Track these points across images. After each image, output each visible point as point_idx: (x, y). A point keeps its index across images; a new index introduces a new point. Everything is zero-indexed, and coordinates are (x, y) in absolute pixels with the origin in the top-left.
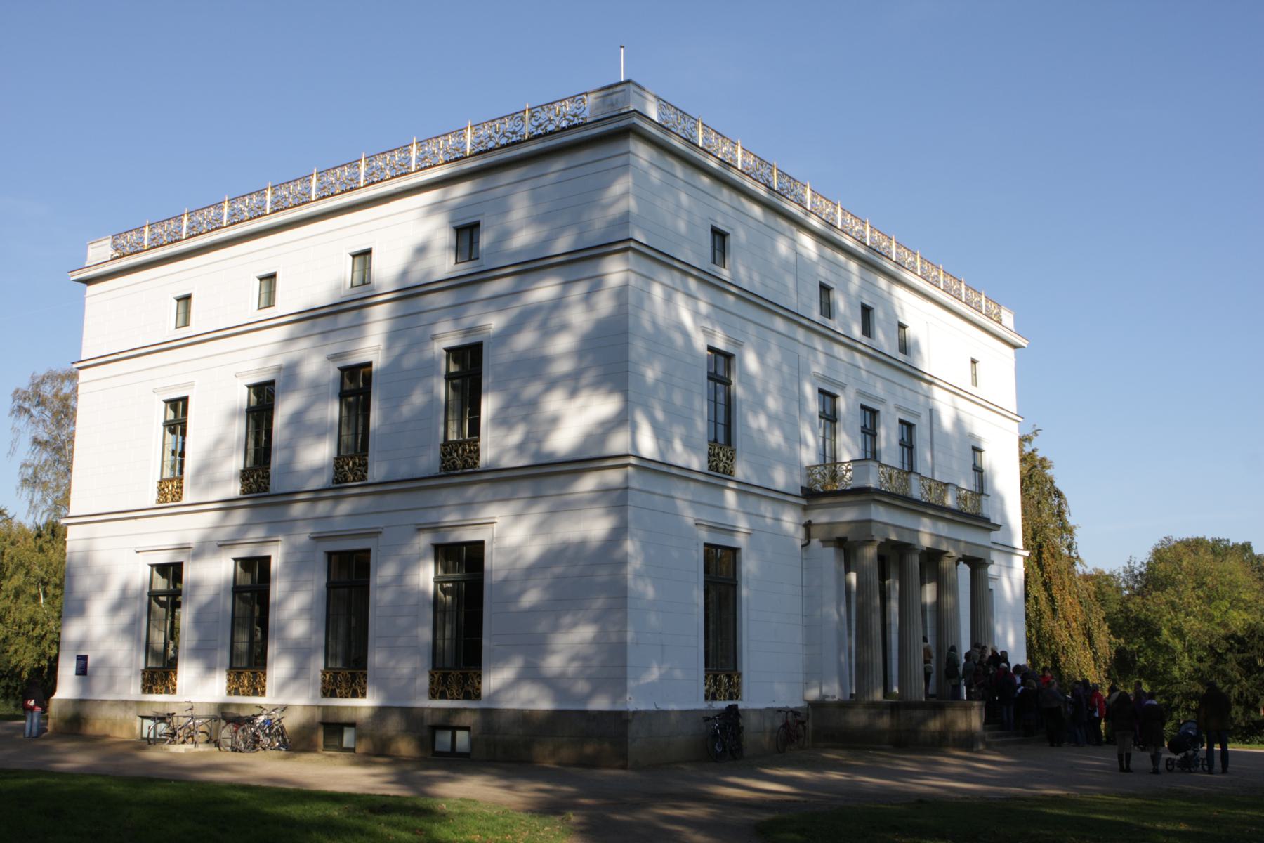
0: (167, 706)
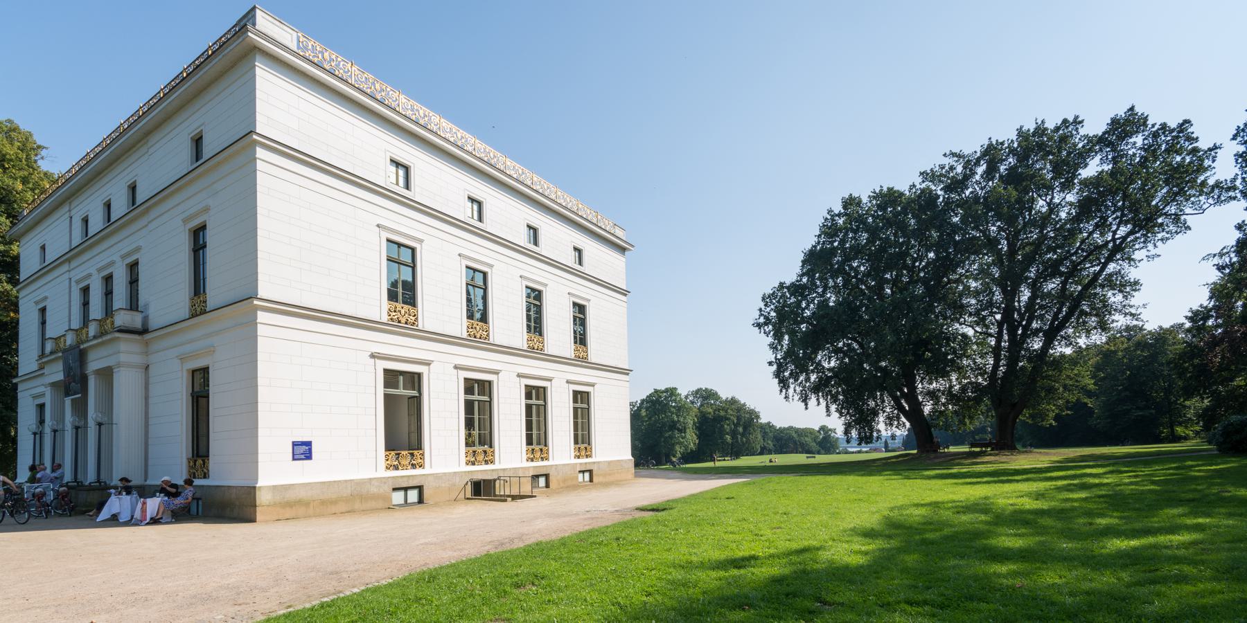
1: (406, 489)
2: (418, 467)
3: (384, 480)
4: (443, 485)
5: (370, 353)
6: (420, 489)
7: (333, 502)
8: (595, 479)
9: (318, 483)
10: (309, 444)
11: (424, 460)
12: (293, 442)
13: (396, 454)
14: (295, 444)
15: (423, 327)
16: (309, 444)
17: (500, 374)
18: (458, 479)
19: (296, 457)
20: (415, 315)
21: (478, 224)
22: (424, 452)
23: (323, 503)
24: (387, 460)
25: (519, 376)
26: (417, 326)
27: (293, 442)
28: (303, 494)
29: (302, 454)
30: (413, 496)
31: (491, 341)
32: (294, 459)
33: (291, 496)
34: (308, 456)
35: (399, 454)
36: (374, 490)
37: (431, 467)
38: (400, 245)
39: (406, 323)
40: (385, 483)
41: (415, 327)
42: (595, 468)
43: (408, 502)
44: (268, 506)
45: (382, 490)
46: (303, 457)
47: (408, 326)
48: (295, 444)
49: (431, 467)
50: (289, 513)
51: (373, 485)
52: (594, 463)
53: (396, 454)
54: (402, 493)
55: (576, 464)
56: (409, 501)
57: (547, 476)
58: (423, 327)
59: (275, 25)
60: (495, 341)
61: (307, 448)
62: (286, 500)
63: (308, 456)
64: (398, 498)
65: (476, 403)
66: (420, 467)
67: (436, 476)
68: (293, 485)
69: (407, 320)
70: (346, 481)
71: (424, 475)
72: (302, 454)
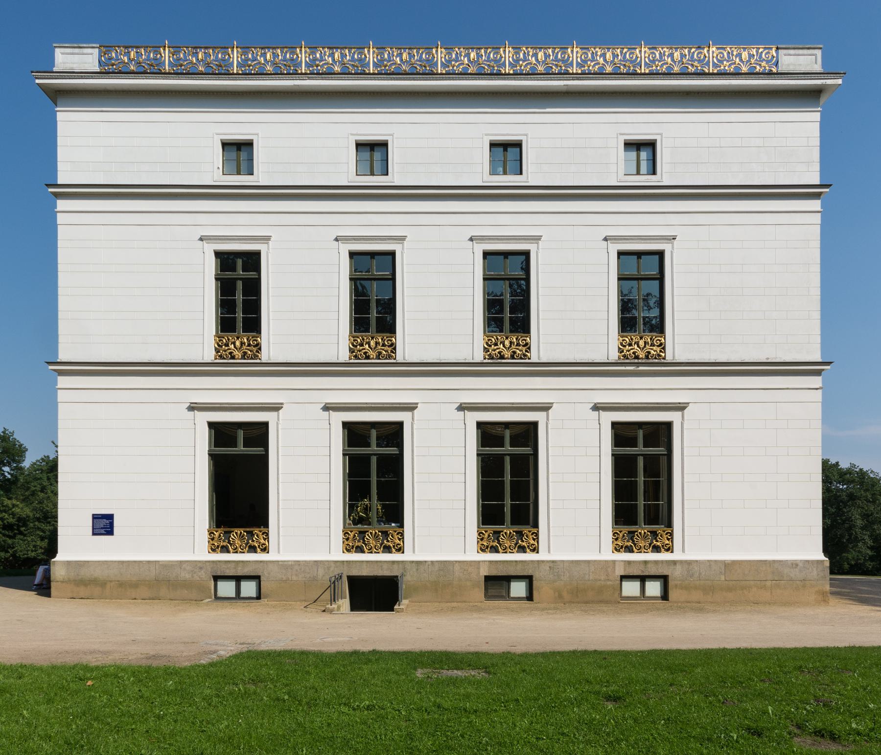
0: (649, 565)
1: (238, 579)
2: (394, 550)
3: (199, 565)
4: (294, 578)
5: (457, 405)
6: (529, 579)
7: (135, 585)
8: (672, 594)
9: (115, 561)
10: (110, 517)
11: (672, 542)
12: (93, 515)
13: (630, 532)
14: (95, 517)
15: (404, 359)
16: (110, 517)
17: (686, 411)
18: (321, 572)
19: (96, 531)
20: (661, 344)
21: (652, 180)
22: (672, 531)
23: (122, 585)
24: (616, 539)
25: (462, 408)
26: (395, 359)
27: (93, 515)
28: (98, 573)
29: (102, 528)
30: (654, 588)
31: (400, 358)
32: (94, 534)
33: (85, 573)
34: (109, 531)
35: (634, 532)
36: (185, 575)
37: (683, 551)
38: (639, 254)
39: (512, 357)
40: (201, 568)
41: (527, 361)
42: (675, 575)
43: (242, 595)
44: (62, 582)
45: (196, 578)
46: (103, 531)
47: (651, 361)
48: (95, 517)
49: (683, 551)
50: (82, 591)
51: (185, 569)
52: (674, 562)
53: (226, 532)
54: (232, 585)
55: (614, 562)
56: (243, 594)
57: (529, 579)
58: (404, 359)
59: (799, 55)
60: (406, 358)
61: (108, 521)
62: (80, 577)
63: (109, 531)
64: (631, 588)
65: (507, 459)
66: (667, 550)
67: (284, 566)
68: (88, 561)
69: (649, 353)
70: (149, 562)
71: (261, 561)
72: (102, 528)
